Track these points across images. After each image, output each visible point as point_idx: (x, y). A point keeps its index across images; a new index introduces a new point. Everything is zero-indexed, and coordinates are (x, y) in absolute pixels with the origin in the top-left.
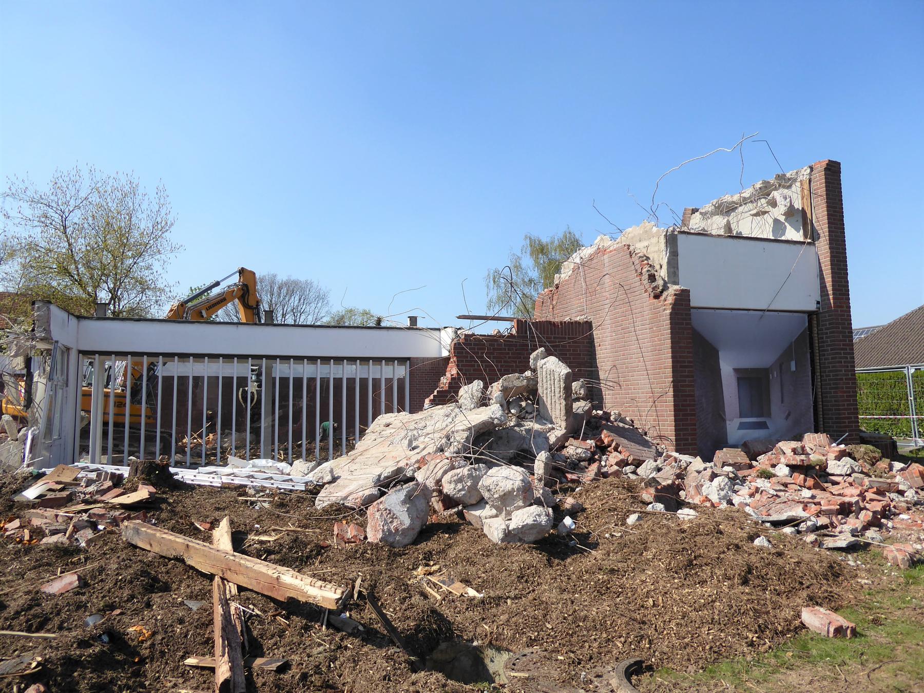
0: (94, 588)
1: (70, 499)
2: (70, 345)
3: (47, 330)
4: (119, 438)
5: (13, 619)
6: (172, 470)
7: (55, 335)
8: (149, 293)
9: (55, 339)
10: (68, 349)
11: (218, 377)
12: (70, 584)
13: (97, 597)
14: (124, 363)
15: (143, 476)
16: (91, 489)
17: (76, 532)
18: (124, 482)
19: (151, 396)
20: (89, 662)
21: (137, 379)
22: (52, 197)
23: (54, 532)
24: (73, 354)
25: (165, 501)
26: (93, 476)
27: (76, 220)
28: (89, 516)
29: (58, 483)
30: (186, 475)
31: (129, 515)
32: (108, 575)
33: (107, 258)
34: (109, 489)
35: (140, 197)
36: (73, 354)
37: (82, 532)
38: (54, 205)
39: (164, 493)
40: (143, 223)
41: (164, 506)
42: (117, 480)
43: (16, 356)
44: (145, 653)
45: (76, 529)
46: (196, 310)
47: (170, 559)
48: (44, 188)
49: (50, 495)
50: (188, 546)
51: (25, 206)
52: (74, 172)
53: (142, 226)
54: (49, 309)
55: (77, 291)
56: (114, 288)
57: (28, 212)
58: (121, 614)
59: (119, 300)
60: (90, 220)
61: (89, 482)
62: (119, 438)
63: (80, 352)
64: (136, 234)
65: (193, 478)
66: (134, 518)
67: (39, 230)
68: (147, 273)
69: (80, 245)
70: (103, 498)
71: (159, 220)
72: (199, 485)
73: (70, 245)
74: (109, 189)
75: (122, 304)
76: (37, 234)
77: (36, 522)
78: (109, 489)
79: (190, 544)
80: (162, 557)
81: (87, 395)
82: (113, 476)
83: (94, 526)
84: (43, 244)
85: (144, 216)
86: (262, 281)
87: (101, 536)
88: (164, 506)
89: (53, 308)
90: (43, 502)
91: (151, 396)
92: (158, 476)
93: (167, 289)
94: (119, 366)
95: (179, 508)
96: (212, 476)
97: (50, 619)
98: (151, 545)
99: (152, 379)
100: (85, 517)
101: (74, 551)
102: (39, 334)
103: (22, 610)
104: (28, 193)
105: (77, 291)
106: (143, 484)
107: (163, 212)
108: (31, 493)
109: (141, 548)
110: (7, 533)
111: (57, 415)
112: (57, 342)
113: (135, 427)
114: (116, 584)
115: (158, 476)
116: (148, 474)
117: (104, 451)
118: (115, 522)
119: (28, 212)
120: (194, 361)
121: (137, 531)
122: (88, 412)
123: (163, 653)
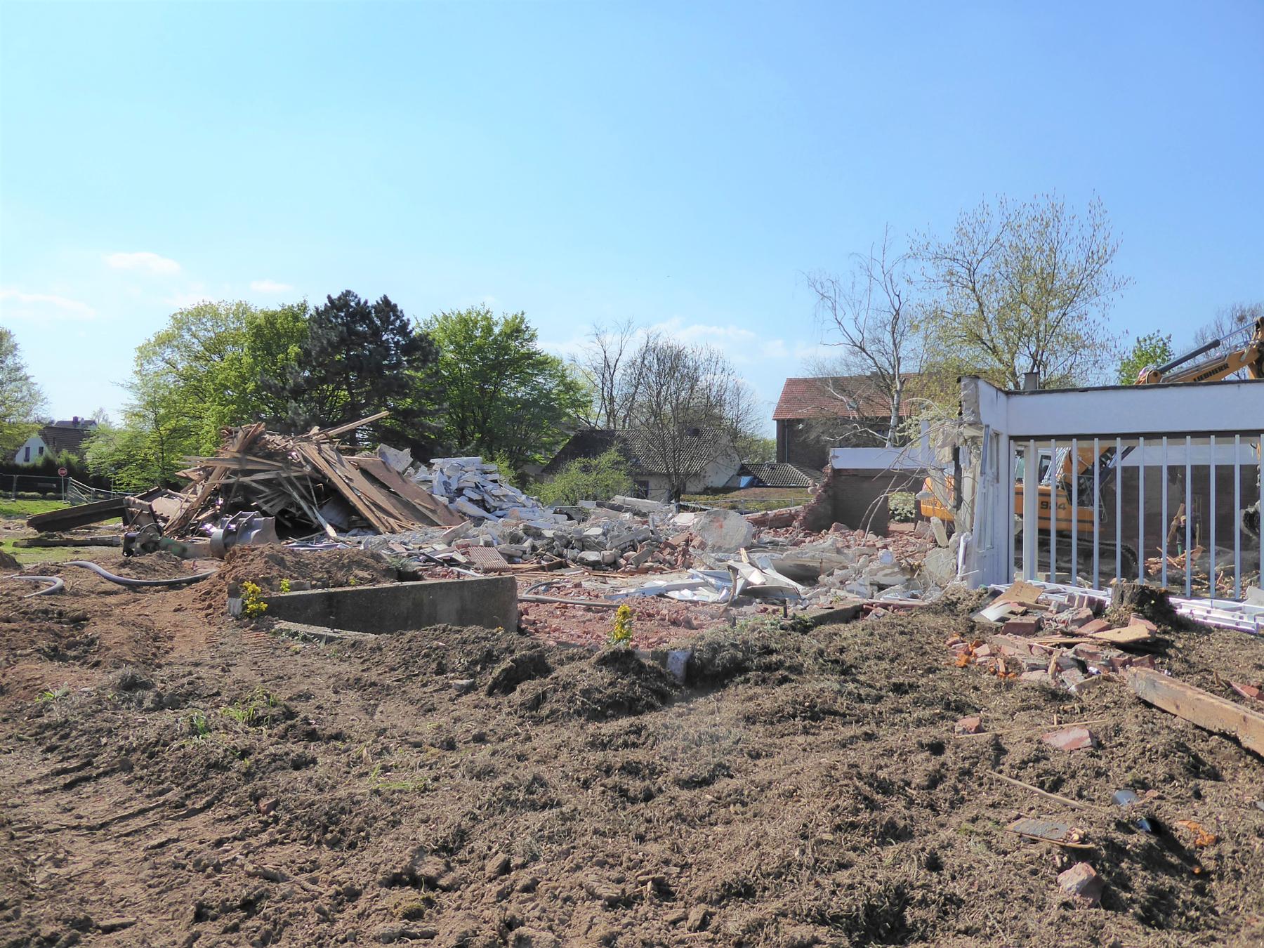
0: (1112, 753)
1: (1037, 628)
2: (1000, 430)
3: (976, 413)
4: (1064, 550)
5: (1020, 769)
6: (1172, 600)
7: (985, 419)
8: (1085, 352)
9: (985, 422)
10: (997, 435)
11: (1233, 467)
12: (1081, 739)
13: (1119, 766)
14: (1066, 450)
15: (1133, 605)
16: (1065, 616)
17: (1060, 672)
18: (1107, 611)
19: (1107, 495)
20: (1137, 855)
21: (1087, 473)
22: (957, 248)
23: (1033, 668)
24: (1004, 440)
25: (1170, 644)
26: (1065, 600)
27: (986, 271)
28: (1076, 653)
29: (1021, 604)
30: (1187, 608)
31: (1130, 659)
32: (1127, 738)
33: (1026, 313)
34: (1088, 620)
35: (1068, 221)
36: (1004, 440)
37: (1068, 672)
38: (959, 257)
39: (1165, 632)
40: (1072, 257)
41: (1171, 652)
42: (1098, 609)
43: (943, 446)
44: (1211, 865)
45: (1060, 668)
46: (1159, 372)
47: (1211, 733)
48: (947, 238)
49: (1014, 620)
50: (1245, 719)
51: (928, 264)
52: (980, 211)
53: (1072, 260)
54: (977, 386)
55: (991, 361)
56: (1037, 351)
57: (932, 272)
58: (1160, 798)
59: (1045, 367)
60: (1003, 270)
61: (1061, 608)
62: (1064, 550)
63: (1011, 438)
64: (1063, 275)
65: (1205, 614)
66: (1137, 664)
67: (944, 291)
68: (1078, 325)
69: (993, 303)
70: (1082, 630)
71: (1095, 248)
72: (1218, 627)
73: (980, 305)
74: (1024, 221)
75: (1049, 370)
76: (942, 298)
77: (1008, 651)
78: (1088, 620)
79: (1249, 716)
80: (1197, 727)
81: (1019, 493)
82: (1091, 602)
83: (1083, 667)
84: (949, 308)
85: (1073, 247)
86: (935, 353)
87: (1095, 683)
88: (1171, 652)
89: (981, 383)
90: (1006, 626)
91: (1107, 495)
92: (1155, 605)
93: (1111, 344)
94: (1060, 452)
95: (1194, 658)
96: (1238, 613)
97: (1064, 781)
98: (1177, 707)
99: (1107, 474)
100: (1070, 653)
101: (1063, 695)
102: (967, 418)
103: (1029, 761)
104: (931, 249)
105: (991, 361)
106: (1138, 617)
107: (1100, 236)
108: (991, 614)
109: (1159, 708)
110: (979, 660)
111: (989, 519)
112: (988, 426)
113: (1085, 538)
114: (1143, 753)
115: (1155, 605)
116: (1141, 603)
117: (1043, 566)
118: (1111, 665)
119: (932, 272)
120: (1241, 442)
121: (1153, 684)
122: (1021, 516)
123: (1237, 875)
